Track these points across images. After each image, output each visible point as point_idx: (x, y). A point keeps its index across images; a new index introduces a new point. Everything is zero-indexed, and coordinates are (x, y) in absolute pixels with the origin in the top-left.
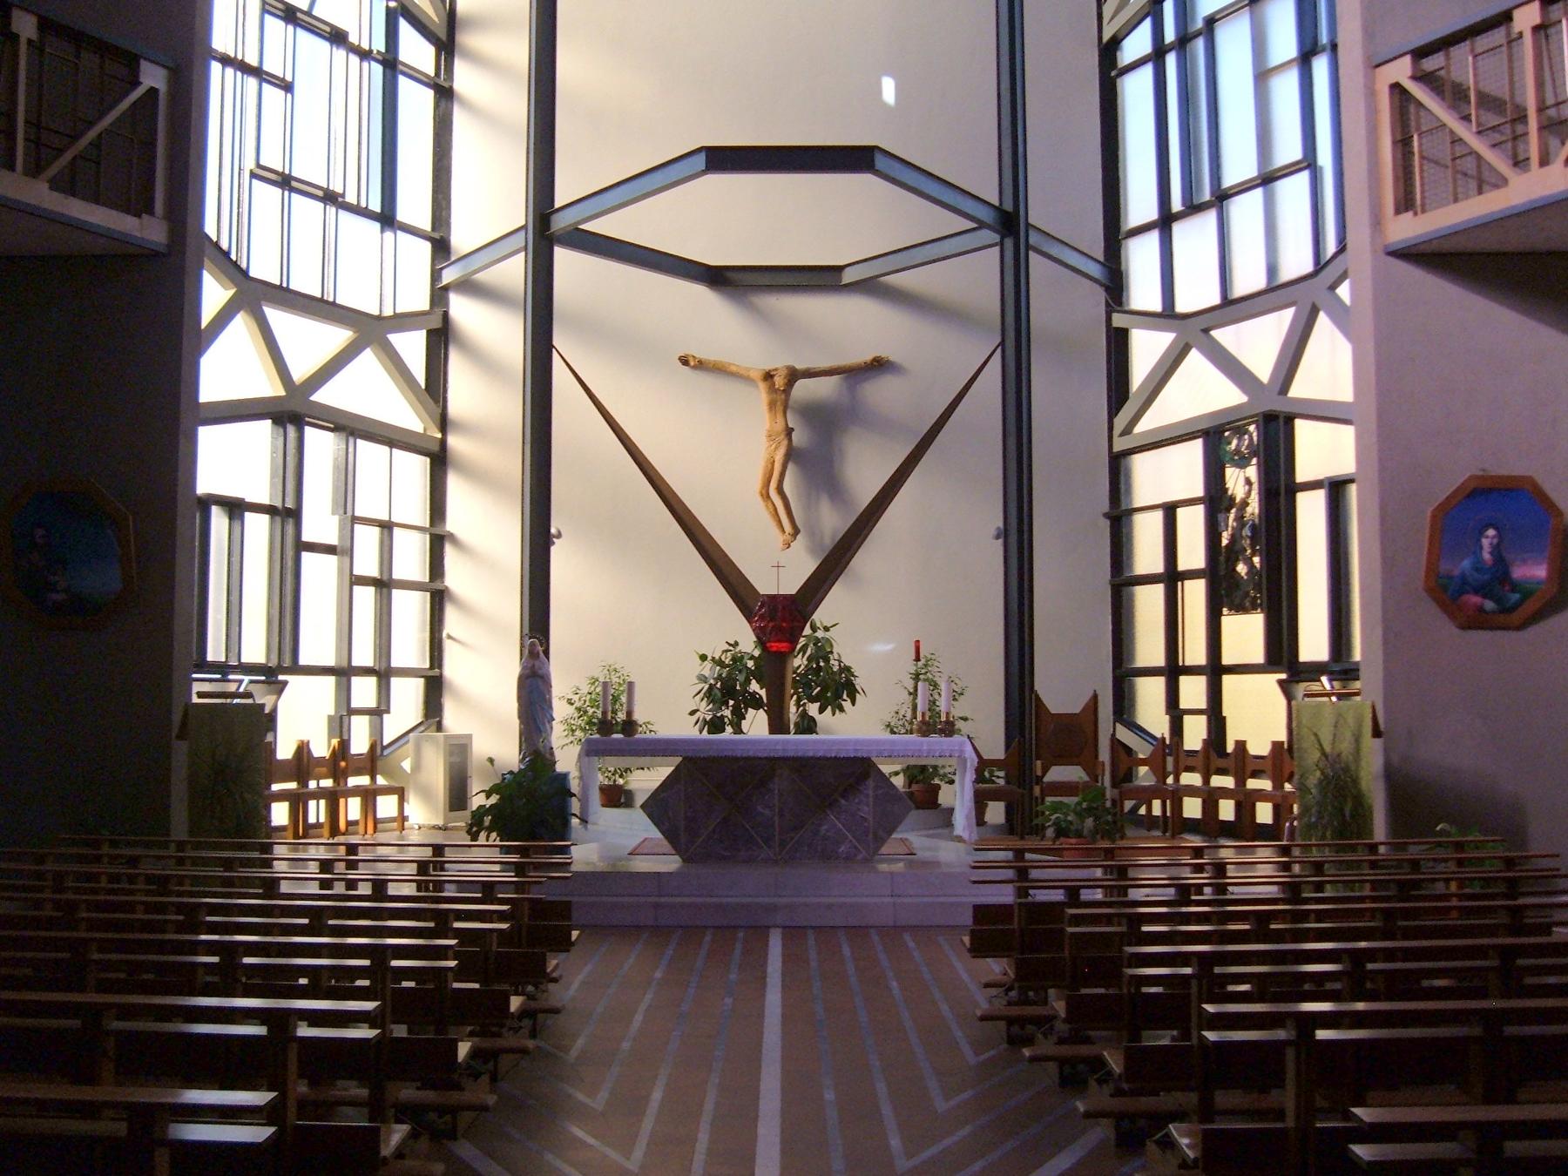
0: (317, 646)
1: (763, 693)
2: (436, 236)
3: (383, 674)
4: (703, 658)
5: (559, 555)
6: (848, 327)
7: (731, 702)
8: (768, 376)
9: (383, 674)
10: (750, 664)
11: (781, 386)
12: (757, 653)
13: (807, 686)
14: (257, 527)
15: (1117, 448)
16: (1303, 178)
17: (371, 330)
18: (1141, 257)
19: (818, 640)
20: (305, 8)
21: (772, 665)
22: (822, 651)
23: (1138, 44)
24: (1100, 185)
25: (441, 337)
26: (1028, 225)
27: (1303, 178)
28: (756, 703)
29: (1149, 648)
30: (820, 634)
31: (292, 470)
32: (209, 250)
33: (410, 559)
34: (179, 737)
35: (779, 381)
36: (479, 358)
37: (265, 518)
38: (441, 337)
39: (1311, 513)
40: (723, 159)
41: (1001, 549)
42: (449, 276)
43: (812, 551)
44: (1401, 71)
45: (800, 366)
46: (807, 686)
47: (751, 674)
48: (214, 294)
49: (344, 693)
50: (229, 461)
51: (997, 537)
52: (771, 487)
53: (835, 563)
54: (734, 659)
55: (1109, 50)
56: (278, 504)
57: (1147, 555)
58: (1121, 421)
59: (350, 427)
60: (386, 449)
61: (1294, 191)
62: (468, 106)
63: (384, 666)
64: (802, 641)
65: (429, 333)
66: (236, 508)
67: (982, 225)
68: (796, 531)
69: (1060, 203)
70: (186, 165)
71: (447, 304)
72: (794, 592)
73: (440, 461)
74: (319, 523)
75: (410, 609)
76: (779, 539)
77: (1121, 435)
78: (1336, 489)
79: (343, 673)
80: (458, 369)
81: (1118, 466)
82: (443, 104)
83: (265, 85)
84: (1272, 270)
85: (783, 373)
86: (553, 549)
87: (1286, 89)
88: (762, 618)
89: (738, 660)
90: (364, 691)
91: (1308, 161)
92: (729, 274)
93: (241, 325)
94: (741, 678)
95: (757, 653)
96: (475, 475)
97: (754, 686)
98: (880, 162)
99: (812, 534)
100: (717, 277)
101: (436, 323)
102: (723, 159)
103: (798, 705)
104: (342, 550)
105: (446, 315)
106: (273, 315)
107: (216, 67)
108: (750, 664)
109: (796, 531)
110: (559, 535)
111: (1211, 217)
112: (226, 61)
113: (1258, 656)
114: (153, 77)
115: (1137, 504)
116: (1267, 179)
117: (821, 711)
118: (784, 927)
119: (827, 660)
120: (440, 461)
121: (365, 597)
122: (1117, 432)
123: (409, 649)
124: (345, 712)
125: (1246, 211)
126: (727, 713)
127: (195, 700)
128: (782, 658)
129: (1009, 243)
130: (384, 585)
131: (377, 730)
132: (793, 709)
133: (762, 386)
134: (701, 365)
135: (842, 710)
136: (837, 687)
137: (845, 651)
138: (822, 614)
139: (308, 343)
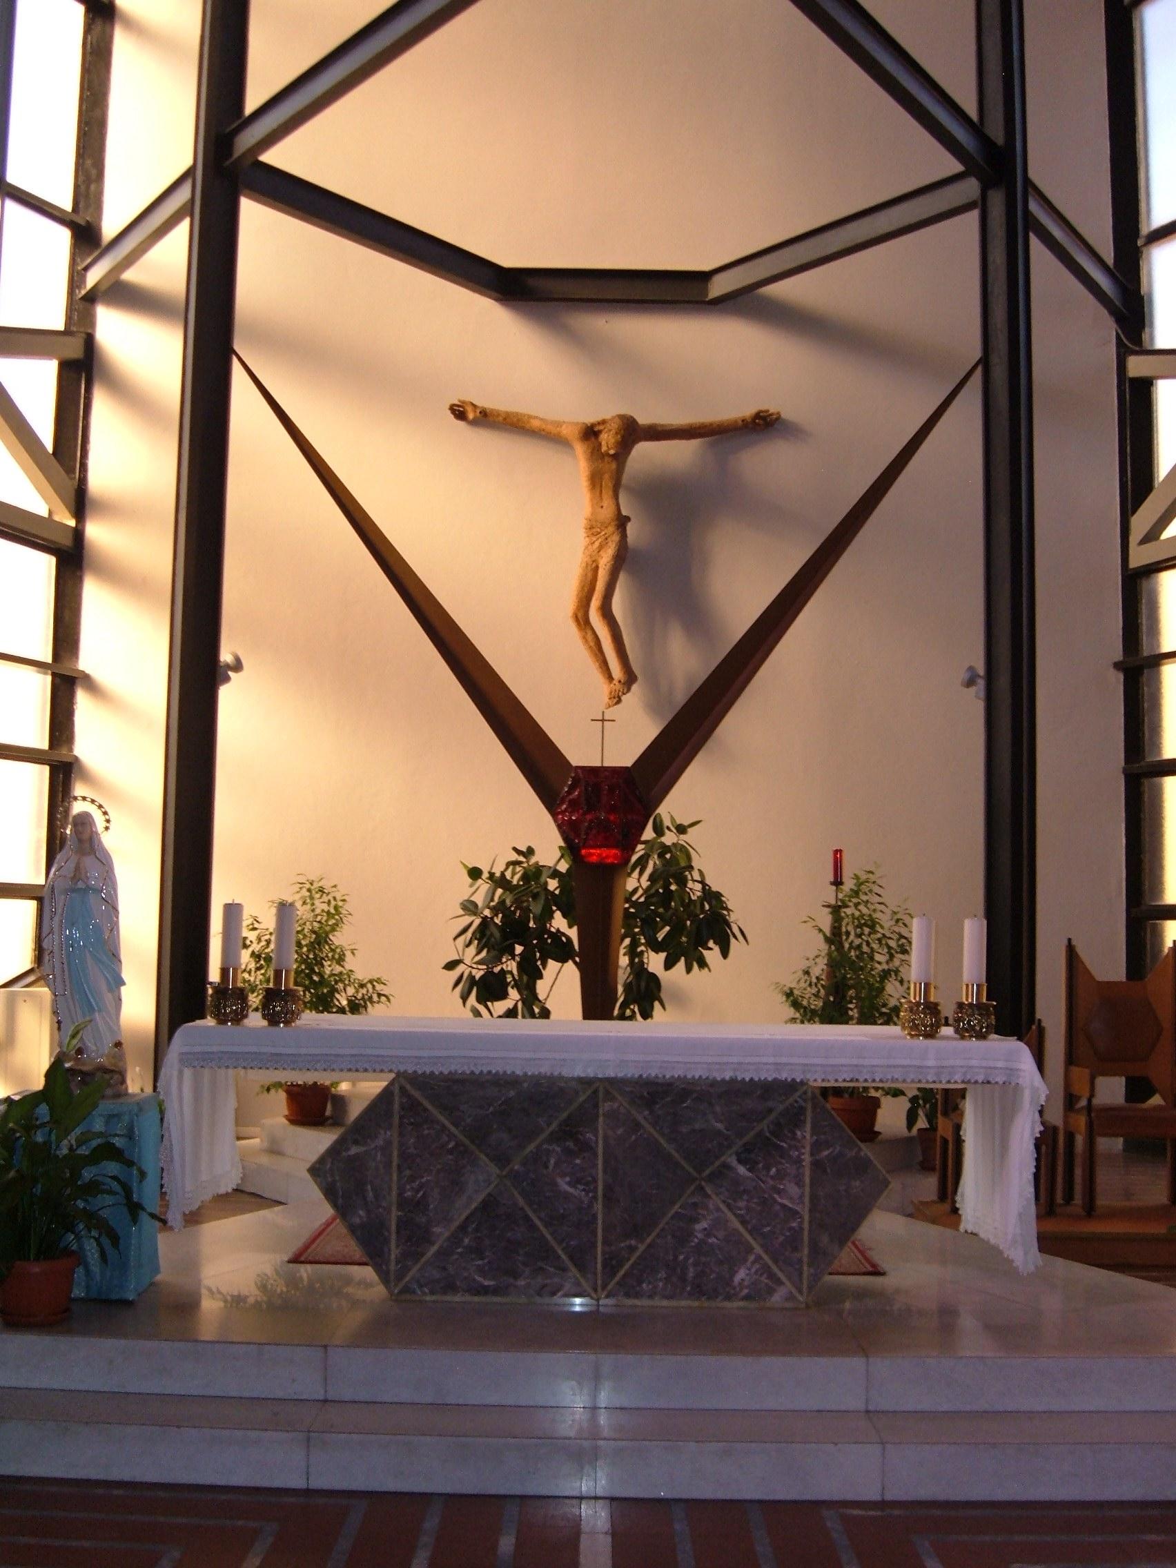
1: (573, 933)
4: (475, 873)
5: (233, 705)
6: (715, 364)
7: (519, 949)
8: (590, 433)
10: (553, 884)
11: (612, 447)
12: (563, 867)
13: (650, 927)
15: (1134, 563)
19: (665, 849)
21: (588, 888)
22: (675, 866)
24: (1107, 165)
25: (81, 370)
26: (1027, 182)
28: (562, 951)
30: (669, 838)
35: (608, 440)
36: (131, 396)
38: (81, 370)
41: (980, 706)
43: (653, 707)
45: (643, 420)
46: (650, 927)
47: (552, 901)
51: (970, 683)
52: (591, 602)
53: (688, 731)
54: (525, 877)
58: (1141, 522)
62: (132, 25)
64: (640, 849)
67: (977, 129)
68: (630, 678)
73: (72, 560)
76: (603, 690)
77: (1144, 541)
80: (105, 417)
82: (98, 27)
85: (614, 426)
88: (574, 805)
89: (534, 875)
92: (532, 282)
94: (536, 908)
95: (563, 867)
96: (115, 576)
97: (559, 922)
99: (654, 684)
100: (514, 287)
101: (74, 350)
103: (633, 952)
105: (90, 342)
108: (553, 884)
109: (630, 678)
110: (238, 666)
117: (669, 965)
118: (612, 1499)
119: (682, 882)
120: (72, 560)
122: (1134, 538)
126: (512, 966)
128: (610, 874)
129: (997, 200)
132: (624, 961)
133: (580, 449)
134: (485, 419)
135: (703, 964)
136: (699, 926)
137: (717, 864)
138: (674, 806)
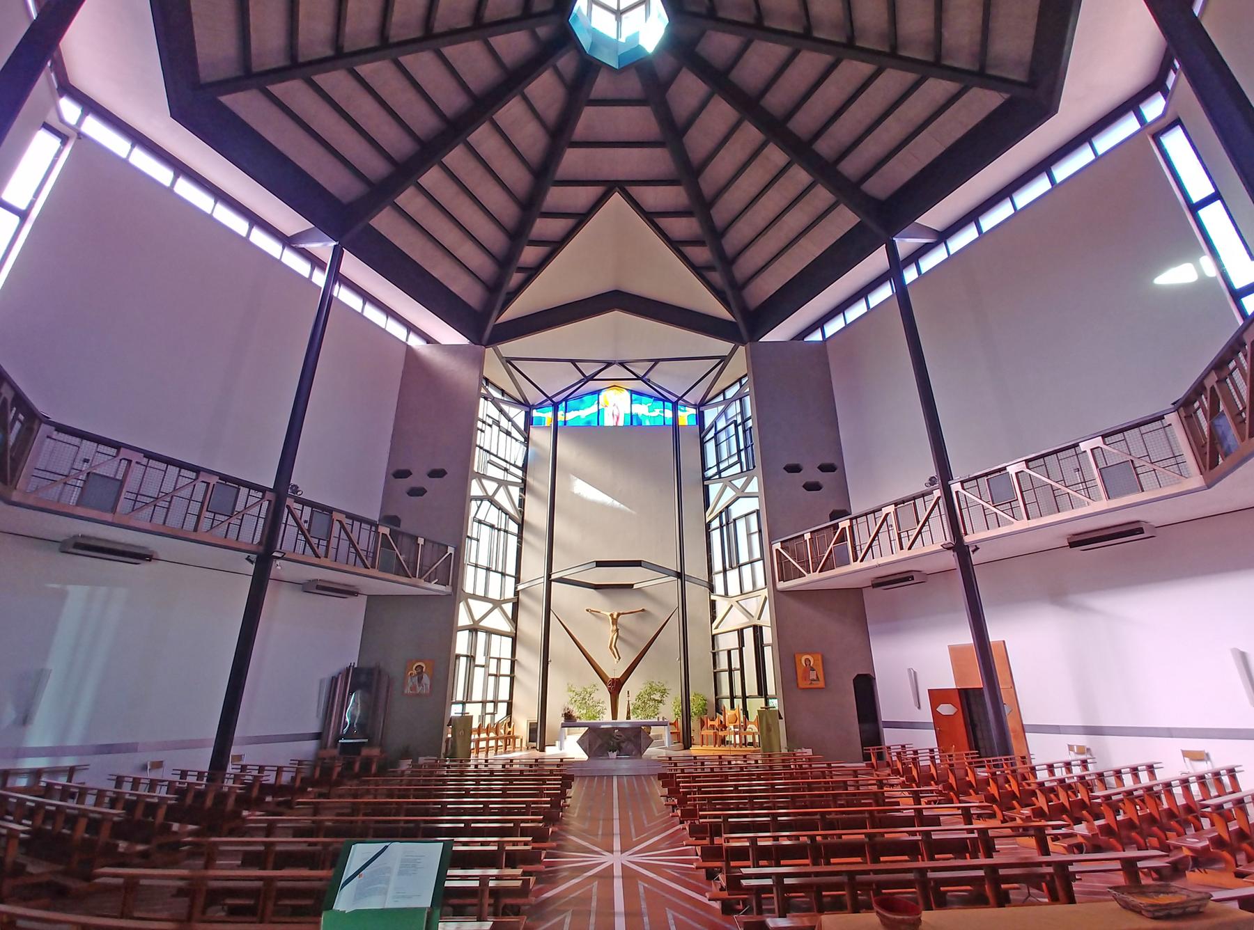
0: (477, 695)
14: (463, 660)
17: (497, 604)
18: (718, 580)
23: (715, 524)
29: (725, 691)
40: (600, 564)
44: (778, 546)
49: (484, 707)
50: (462, 642)
55: (708, 525)
57: (723, 664)
59: (490, 632)
69: (695, 568)
72: (667, 21)
74: (480, 659)
75: (505, 683)
79: (484, 703)
87: (755, 538)
100: (596, 587)
114: (451, 550)
121: (492, 679)
123: (504, 694)
125: (746, 570)
131: (493, 719)
139: (479, 608)
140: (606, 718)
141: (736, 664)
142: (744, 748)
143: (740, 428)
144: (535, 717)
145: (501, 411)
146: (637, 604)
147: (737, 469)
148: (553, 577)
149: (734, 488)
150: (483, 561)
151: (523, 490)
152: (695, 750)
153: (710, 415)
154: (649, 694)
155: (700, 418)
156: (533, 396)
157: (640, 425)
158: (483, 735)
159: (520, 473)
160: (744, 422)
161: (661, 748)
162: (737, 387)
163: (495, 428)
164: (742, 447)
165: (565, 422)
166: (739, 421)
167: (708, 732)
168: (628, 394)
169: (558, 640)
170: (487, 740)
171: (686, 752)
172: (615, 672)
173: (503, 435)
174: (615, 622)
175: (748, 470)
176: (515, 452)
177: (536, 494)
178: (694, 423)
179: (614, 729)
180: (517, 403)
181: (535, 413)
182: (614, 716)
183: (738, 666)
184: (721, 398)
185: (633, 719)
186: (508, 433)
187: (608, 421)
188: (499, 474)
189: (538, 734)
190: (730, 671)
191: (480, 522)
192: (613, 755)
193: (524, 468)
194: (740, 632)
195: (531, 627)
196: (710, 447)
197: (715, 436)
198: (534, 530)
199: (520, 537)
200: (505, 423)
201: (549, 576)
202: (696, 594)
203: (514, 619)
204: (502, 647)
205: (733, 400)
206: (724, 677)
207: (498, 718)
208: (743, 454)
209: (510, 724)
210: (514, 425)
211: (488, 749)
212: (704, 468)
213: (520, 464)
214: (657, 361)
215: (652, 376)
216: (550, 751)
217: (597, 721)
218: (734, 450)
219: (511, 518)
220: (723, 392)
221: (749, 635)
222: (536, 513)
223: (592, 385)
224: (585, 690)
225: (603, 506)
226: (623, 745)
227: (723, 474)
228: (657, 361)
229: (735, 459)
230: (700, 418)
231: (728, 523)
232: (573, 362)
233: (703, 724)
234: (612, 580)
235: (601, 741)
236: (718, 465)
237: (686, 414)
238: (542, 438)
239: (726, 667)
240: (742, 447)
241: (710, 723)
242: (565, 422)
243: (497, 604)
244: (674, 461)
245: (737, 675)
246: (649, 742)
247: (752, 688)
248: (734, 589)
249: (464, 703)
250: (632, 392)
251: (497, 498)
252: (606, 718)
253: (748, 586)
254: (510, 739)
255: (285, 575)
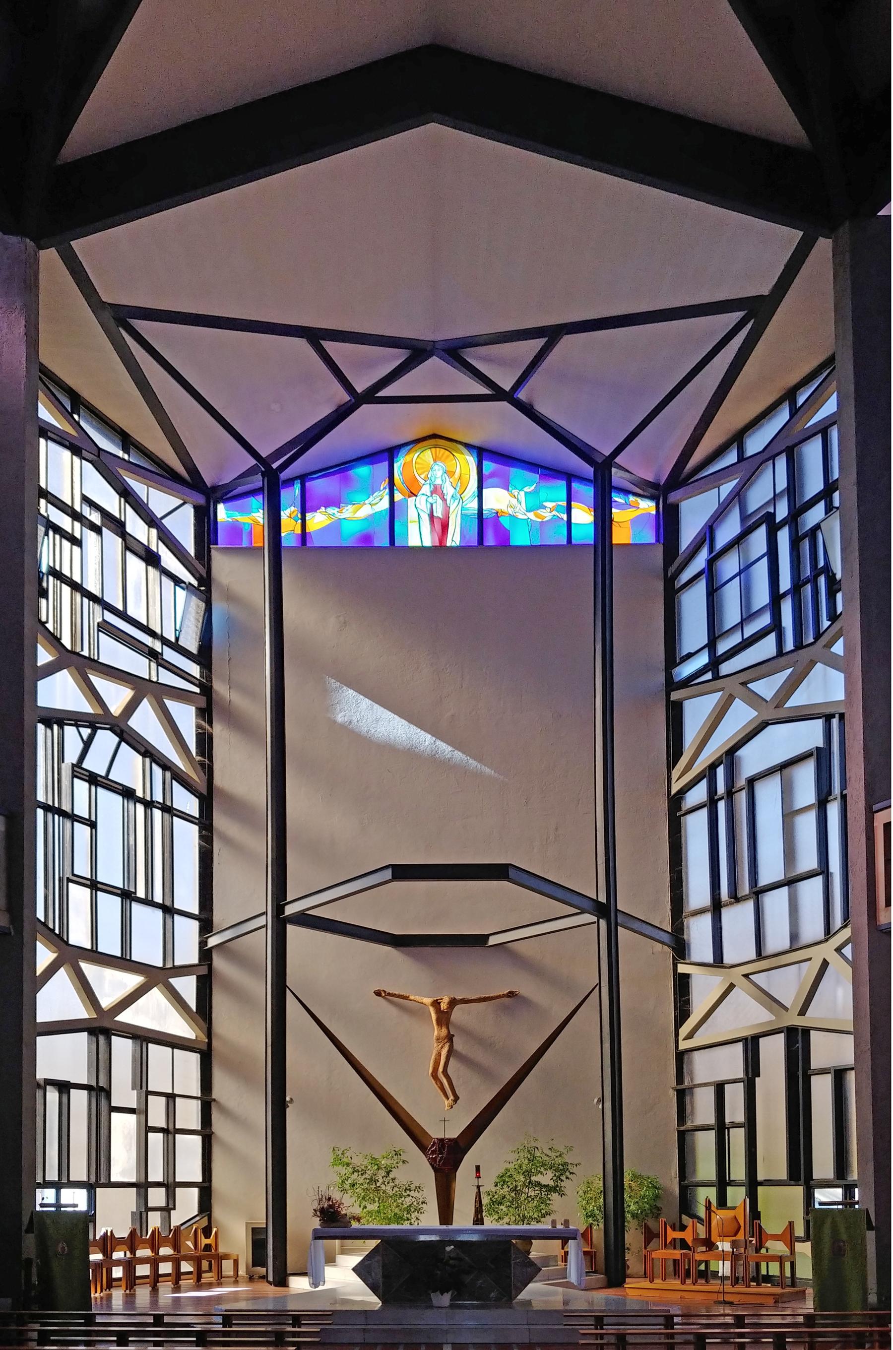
0: (123, 1165)
2: (203, 917)
3: (170, 1186)
9: (170, 1186)
14: (79, 1100)
16: (819, 881)
17: (157, 977)
18: (699, 931)
20: (103, 774)
23: (699, 794)
26: (617, 910)
27: (819, 881)
29: (706, 1169)
31: (101, 1063)
32: (39, 926)
33: (189, 1114)
34: (27, 1232)
37: (85, 1093)
39: (822, 1090)
40: (402, 872)
42: (213, 941)
45: (459, 997)
48: (44, 956)
49: (143, 1197)
50: (60, 1058)
55: (675, 801)
56: (94, 1084)
57: (703, 1109)
58: (684, 1030)
59: (143, 1038)
60: (170, 1049)
61: (812, 890)
63: (171, 1180)
65: (198, 977)
66: (64, 1087)
68: (456, 1099)
69: (641, 895)
70: (276, 657)
71: (211, 960)
74: (123, 1092)
75: (189, 1149)
78: (839, 1075)
79: (142, 1186)
80: (220, 1002)
81: (681, 1057)
83: (75, 823)
84: (794, 936)
86: (288, 1110)
87: (807, 825)
90: (157, 1197)
91: (823, 870)
93: (62, 976)
98: (512, 873)
101: (204, 971)
102: (402, 872)
104: (141, 1111)
105: (210, 967)
106: (86, 967)
107: (40, 812)
111: (748, 907)
112: (47, 808)
113: (783, 1175)
115: (698, 1081)
116: (791, 882)
118: (452, 1344)
121: (156, 1140)
122: (681, 1037)
123: (189, 1167)
124: (143, 1210)
125: (776, 904)
127: (38, 1208)
130: (170, 1132)
139: (111, 985)
140: (429, 1219)
141: (735, 1112)
142: (754, 1288)
143: (783, 537)
144: (261, 1216)
145: (126, 493)
146: (501, 979)
147: (767, 647)
148: (289, 910)
149: (754, 700)
150: (111, 873)
151: (206, 713)
152: (637, 1292)
153: (695, 513)
154: (528, 1173)
155: (668, 522)
156: (218, 459)
157: (503, 536)
158: (143, 1252)
159: (194, 670)
160: (797, 511)
161: (557, 1288)
162: (783, 416)
163: (113, 542)
164: (785, 583)
165: (304, 536)
166: (782, 511)
167: (662, 1254)
168: (467, 463)
169: (306, 1055)
170: (154, 1262)
171: (612, 1293)
172: (445, 1122)
173: (136, 565)
174: (444, 1018)
175: (799, 645)
176: (172, 610)
177: (236, 722)
178: (648, 536)
179: (442, 1244)
180: (165, 476)
181: (223, 513)
182: (446, 1215)
183: (740, 1117)
184: (732, 457)
185: (490, 1223)
186: (151, 559)
187: (417, 534)
188: (139, 665)
189: (272, 1252)
190: (721, 1128)
191: (93, 780)
192: (445, 1299)
193: (204, 656)
194: (751, 1045)
195: (243, 1029)
196: (693, 603)
197: (710, 571)
198: (240, 809)
199: (205, 823)
200: (137, 527)
201: (279, 909)
202: (642, 958)
203: (203, 1012)
204: (176, 1071)
205: (768, 455)
206: (705, 1143)
207: (177, 1218)
208: (787, 608)
209: (207, 1232)
210: (166, 537)
211: (155, 1279)
212: (673, 658)
213: (191, 643)
214: (552, 334)
215: (541, 393)
216: (299, 1284)
217: (406, 1226)
218: (761, 597)
219: (179, 777)
220: (738, 438)
221: (773, 1051)
222: (242, 770)
223: (370, 425)
224: (374, 1161)
225: (409, 755)
226: (468, 1279)
227: (726, 668)
228: (552, 334)
229: (765, 620)
230: (668, 522)
231: (728, 784)
232: (315, 336)
233: (650, 1236)
234: (437, 908)
235: (402, 1267)
236: (711, 645)
237: (631, 514)
238: (241, 576)
239: (711, 1120)
240: (785, 583)
241: (672, 1235)
242: (304, 536)
243: (157, 977)
244: (595, 636)
245: (737, 1139)
246: (531, 1271)
247: (774, 1158)
248: (739, 945)
249: (91, 1187)
250: (482, 453)
251: (135, 722)
252: (429, 1219)
253: (777, 937)
254: (209, 1260)
255: (631, 1341)
